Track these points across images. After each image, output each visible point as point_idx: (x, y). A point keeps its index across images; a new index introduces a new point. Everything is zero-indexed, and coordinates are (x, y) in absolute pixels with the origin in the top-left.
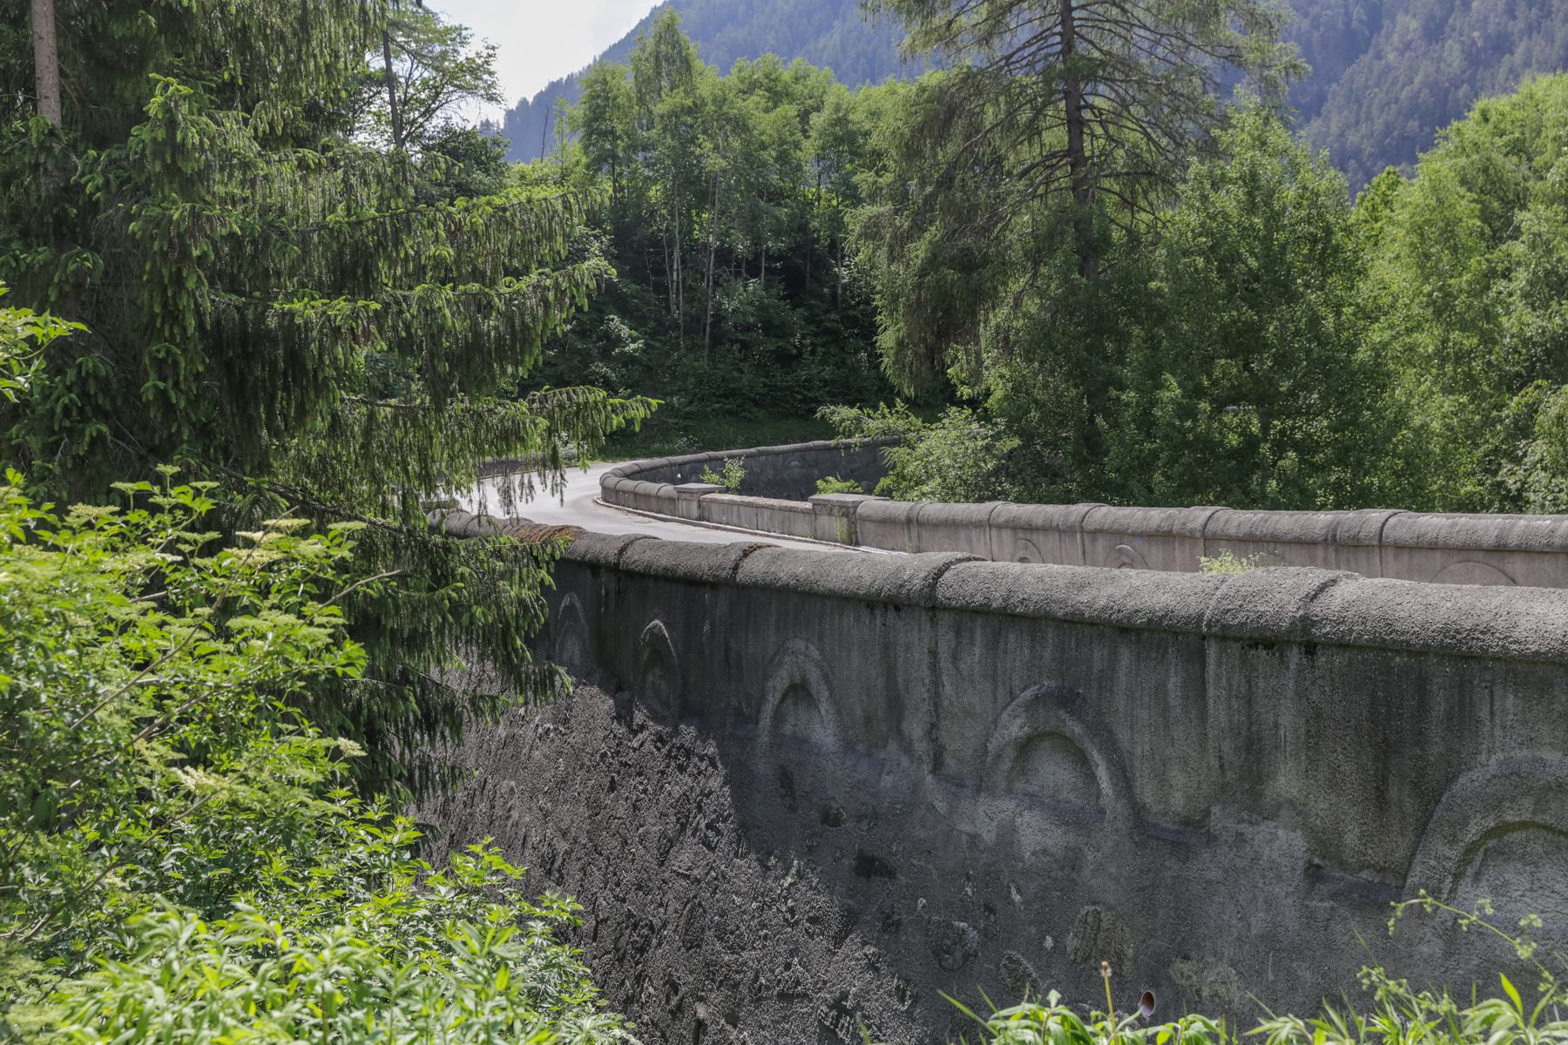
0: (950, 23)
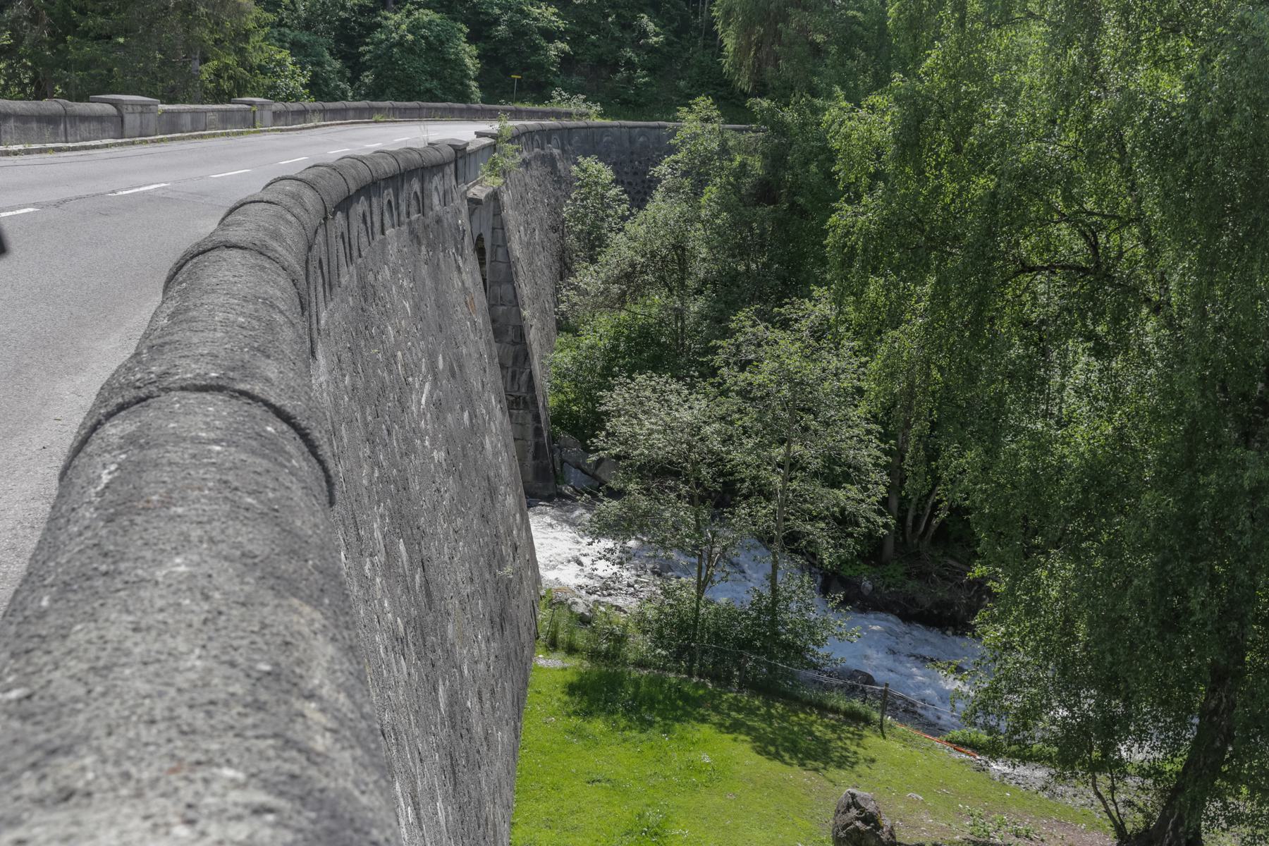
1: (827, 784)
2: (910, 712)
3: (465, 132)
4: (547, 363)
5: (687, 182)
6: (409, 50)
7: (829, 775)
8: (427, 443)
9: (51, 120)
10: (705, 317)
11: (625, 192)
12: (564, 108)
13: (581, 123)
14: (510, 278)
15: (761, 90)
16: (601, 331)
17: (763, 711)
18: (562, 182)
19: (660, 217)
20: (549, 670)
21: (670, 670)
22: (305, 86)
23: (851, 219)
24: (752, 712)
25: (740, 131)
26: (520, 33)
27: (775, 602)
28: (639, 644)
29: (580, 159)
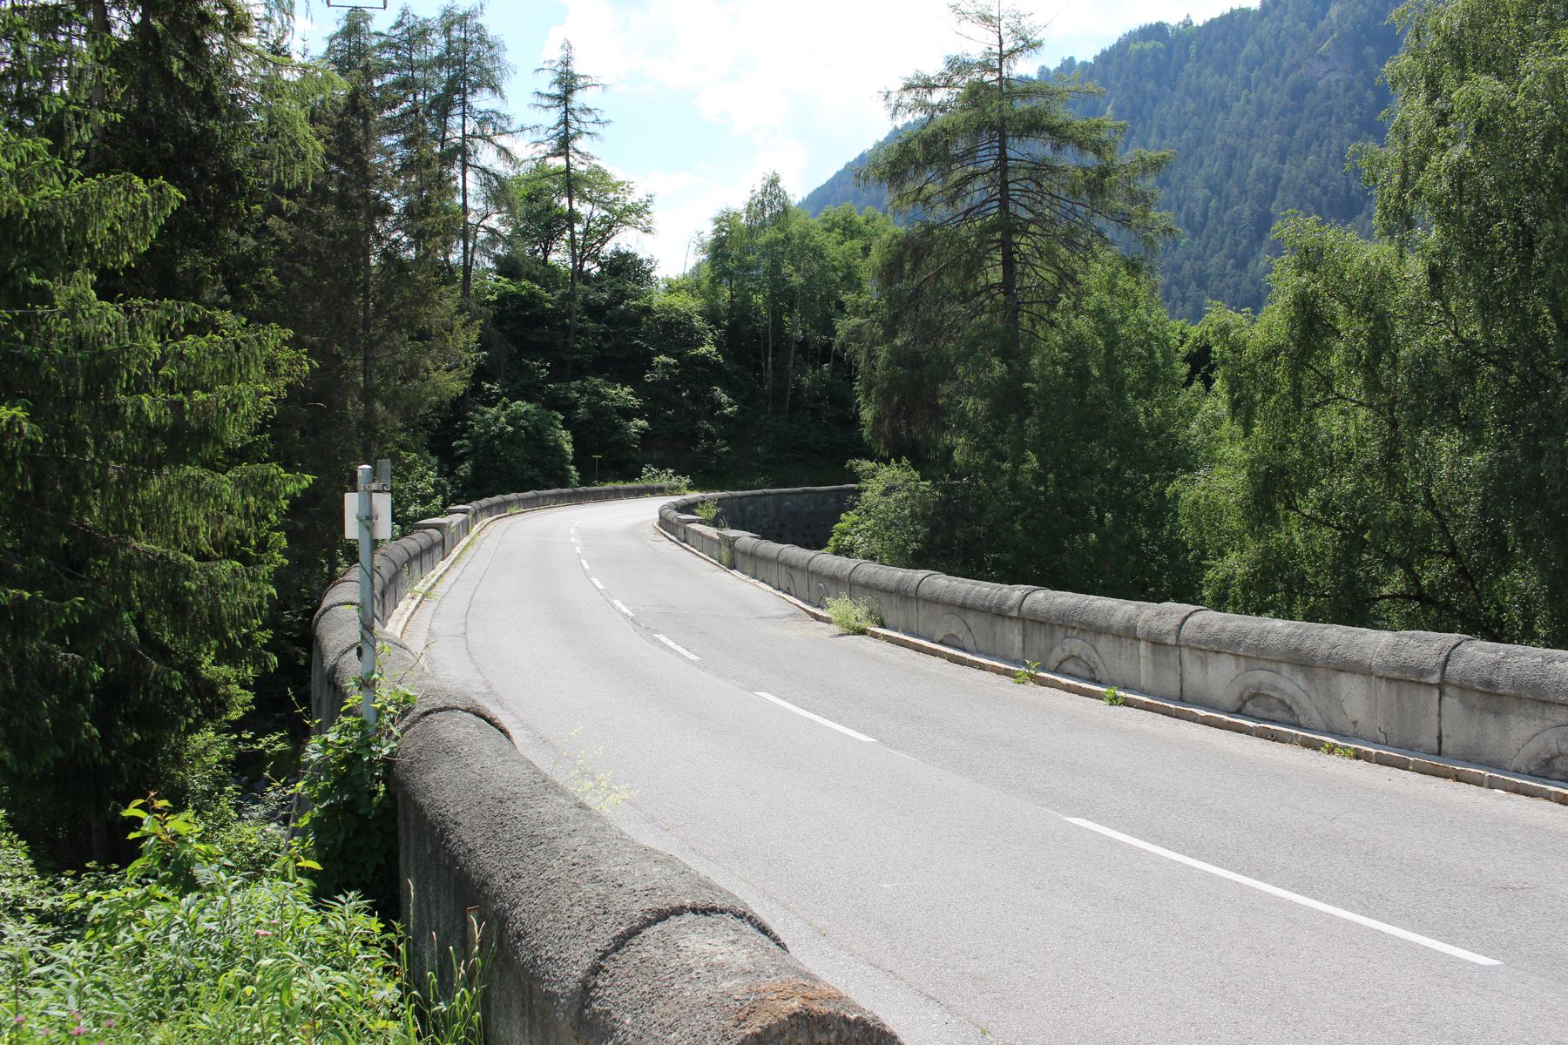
0: (920, 190)
6: (510, 440)
12: (657, 483)
26: (598, 413)
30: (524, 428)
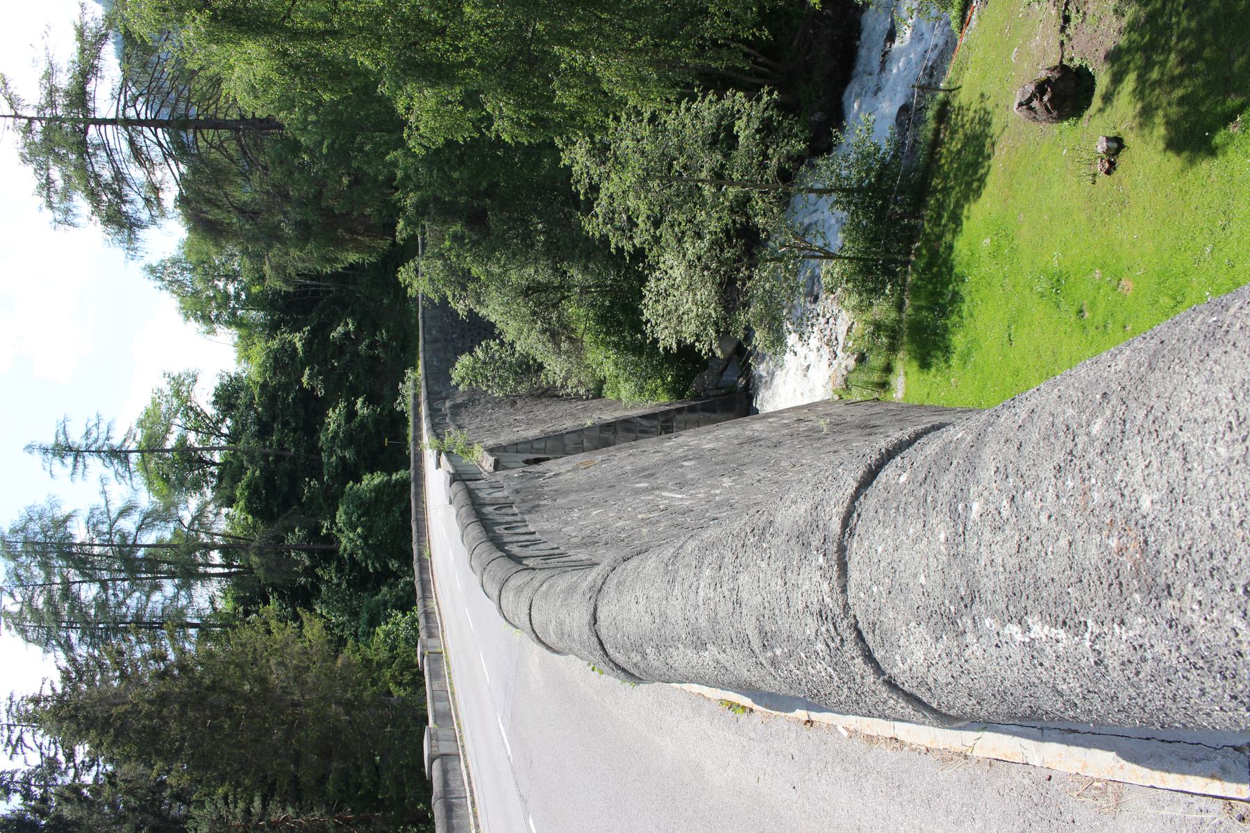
1: (1006, 133)
2: (934, 71)
3: (436, 482)
4: (631, 404)
5: (471, 286)
7: (998, 132)
8: (717, 492)
9: (449, 809)
10: (586, 268)
11: (480, 345)
12: (410, 400)
13: (423, 384)
14: (559, 437)
15: (390, 228)
16: (601, 357)
17: (939, 196)
18: (473, 398)
19: (501, 309)
20: (907, 388)
21: (905, 280)
22: (405, 615)
23: (505, 121)
24: (941, 206)
25: (424, 245)
26: (350, 439)
27: (843, 190)
28: (882, 309)
29: (453, 383)
30: (359, 517)
